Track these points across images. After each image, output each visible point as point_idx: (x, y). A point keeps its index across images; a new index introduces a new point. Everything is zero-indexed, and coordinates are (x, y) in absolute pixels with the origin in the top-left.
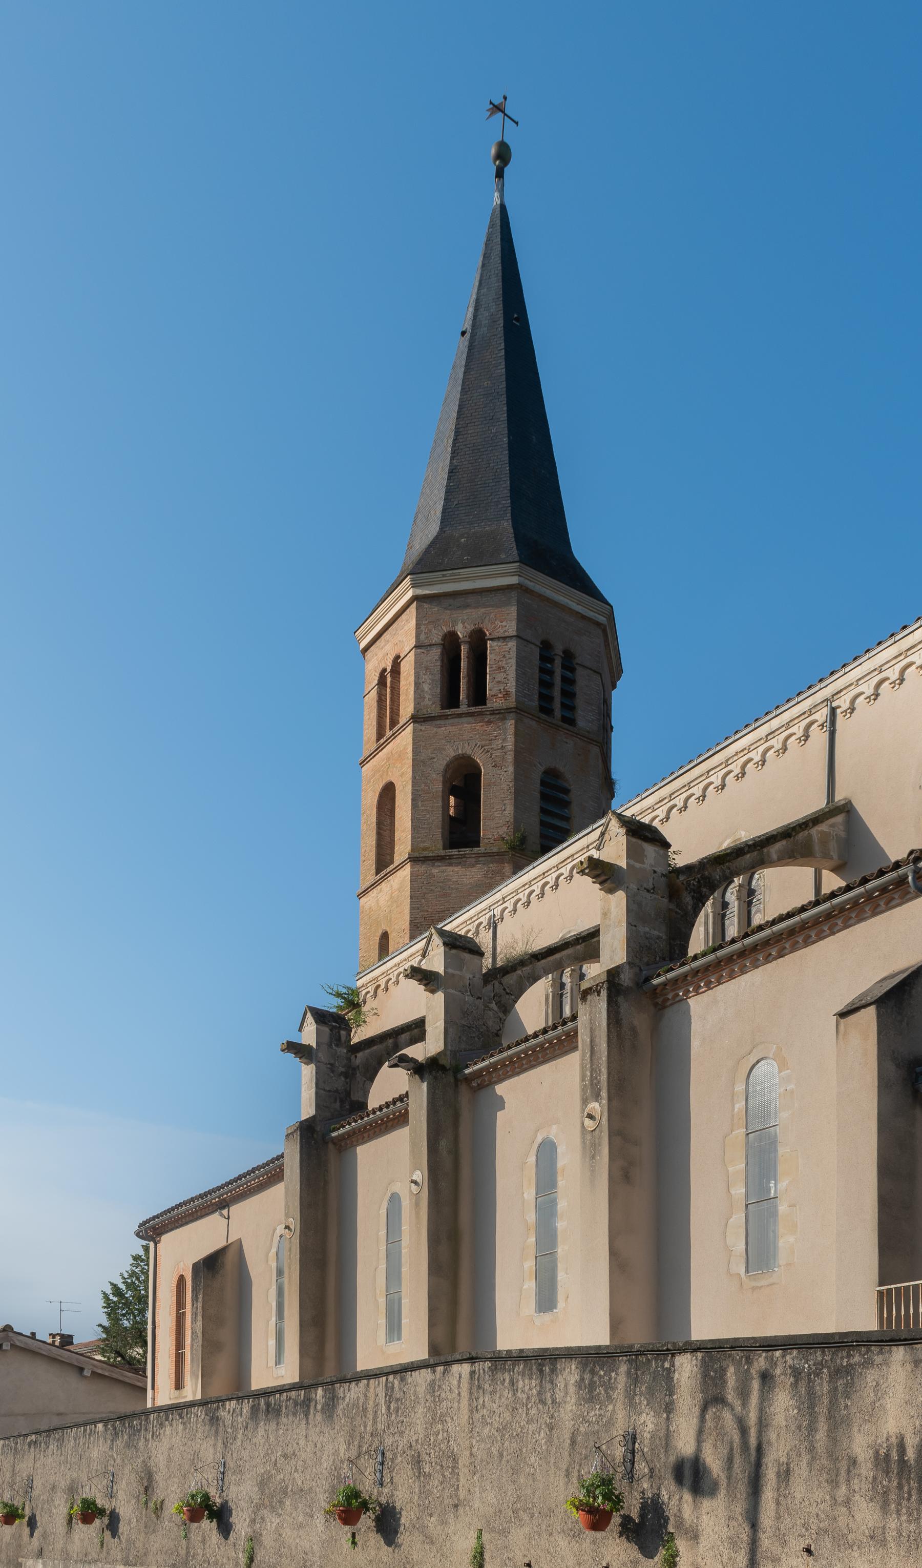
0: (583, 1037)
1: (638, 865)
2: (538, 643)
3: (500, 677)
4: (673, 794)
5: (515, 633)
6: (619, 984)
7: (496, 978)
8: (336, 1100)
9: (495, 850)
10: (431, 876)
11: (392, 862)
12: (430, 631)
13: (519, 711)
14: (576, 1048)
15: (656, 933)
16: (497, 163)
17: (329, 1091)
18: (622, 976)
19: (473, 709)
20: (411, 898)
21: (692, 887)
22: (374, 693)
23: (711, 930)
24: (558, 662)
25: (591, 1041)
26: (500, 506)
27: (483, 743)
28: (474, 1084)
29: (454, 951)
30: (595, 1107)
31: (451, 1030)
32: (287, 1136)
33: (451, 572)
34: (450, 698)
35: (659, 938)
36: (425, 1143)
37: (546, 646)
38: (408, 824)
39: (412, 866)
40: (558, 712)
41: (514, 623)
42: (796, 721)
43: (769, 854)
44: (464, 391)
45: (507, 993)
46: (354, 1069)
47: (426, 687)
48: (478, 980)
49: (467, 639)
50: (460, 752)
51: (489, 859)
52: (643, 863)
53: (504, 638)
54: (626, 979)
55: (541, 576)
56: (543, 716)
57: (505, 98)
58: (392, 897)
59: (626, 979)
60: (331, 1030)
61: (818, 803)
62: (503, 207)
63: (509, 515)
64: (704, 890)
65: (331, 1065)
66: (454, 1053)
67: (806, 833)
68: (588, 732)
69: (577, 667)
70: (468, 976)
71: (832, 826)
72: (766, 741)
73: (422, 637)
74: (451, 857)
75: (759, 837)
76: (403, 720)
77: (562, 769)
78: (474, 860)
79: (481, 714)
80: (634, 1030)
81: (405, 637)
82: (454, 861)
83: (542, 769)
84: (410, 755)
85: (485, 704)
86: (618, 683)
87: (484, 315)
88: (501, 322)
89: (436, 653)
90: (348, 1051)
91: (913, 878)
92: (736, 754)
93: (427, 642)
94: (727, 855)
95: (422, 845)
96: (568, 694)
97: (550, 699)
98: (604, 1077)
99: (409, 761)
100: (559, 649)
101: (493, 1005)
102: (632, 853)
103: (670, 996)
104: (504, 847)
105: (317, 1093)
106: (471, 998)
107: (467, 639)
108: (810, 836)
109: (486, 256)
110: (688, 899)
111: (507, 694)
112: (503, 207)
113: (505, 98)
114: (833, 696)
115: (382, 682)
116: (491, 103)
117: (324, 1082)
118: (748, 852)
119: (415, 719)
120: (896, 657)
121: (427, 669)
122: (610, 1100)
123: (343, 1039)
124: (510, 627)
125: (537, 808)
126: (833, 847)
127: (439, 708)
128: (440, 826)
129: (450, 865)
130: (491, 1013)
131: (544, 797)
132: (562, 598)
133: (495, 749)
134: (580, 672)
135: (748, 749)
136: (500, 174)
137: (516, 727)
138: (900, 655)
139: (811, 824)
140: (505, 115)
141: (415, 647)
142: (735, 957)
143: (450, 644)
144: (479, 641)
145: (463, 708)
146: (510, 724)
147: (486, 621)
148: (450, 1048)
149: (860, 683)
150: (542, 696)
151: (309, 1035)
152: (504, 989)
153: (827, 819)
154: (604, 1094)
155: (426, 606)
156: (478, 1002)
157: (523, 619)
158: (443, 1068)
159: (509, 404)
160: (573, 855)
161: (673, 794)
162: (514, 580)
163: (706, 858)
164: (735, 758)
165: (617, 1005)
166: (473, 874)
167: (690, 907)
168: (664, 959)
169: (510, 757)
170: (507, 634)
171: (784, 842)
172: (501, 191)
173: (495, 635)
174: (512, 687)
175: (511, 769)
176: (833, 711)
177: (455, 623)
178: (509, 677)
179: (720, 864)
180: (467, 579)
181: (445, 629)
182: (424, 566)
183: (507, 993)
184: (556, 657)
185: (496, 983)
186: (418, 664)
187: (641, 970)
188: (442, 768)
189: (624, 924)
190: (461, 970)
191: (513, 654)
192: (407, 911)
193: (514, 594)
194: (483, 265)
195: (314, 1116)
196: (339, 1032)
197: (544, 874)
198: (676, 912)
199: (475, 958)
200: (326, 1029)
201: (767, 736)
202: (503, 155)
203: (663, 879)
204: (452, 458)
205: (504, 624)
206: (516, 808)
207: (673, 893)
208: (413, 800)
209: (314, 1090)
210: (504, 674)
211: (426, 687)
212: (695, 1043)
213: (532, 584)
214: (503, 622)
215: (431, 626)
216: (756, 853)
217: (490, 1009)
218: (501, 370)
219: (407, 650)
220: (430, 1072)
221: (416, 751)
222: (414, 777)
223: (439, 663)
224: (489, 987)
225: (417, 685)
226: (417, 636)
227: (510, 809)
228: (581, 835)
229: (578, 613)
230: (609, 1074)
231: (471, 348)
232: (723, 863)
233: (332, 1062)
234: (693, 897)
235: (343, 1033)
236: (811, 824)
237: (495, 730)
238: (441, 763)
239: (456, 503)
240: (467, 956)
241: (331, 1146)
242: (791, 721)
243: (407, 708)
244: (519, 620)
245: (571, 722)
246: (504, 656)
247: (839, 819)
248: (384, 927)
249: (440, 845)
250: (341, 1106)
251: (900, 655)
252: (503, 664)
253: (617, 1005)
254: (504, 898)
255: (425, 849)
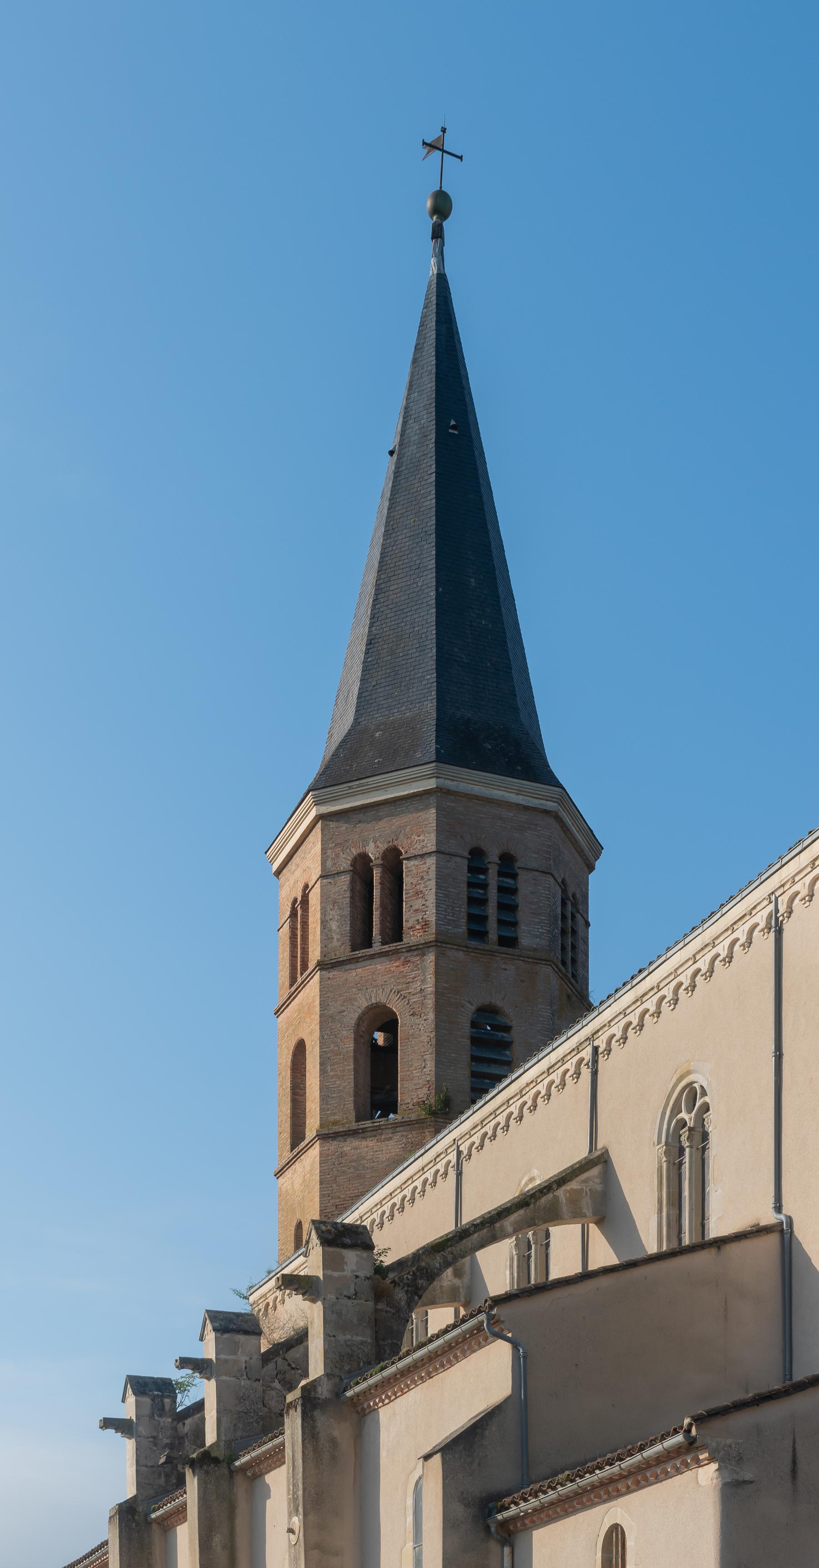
0: (288, 1452)
1: (336, 1274)
2: (466, 854)
3: (418, 904)
4: (484, 1120)
5: (434, 849)
6: (315, 1398)
7: (278, 1355)
8: (160, 1475)
9: (413, 1117)
10: (343, 1155)
11: (303, 1139)
12: (337, 856)
13: (441, 943)
14: (284, 1463)
15: (359, 1338)
16: (435, 218)
17: (152, 1467)
18: (319, 1390)
19: (386, 948)
20: (321, 1183)
21: (405, 1281)
22: (286, 927)
23: (515, 1275)
24: (493, 871)
25: (293, 1456)
26: (424, 682)
27: (400, 987)
28: (249, 1474)
29: (226, 1336)
30: (295, 1519)
31: (224, 1419)
32: (110, 1518)
33: (358, 783)
34: (361, 938)
35: (362, 1343)
36: (197, 1542)
37: (477, 854)
38: (317, 1094)
39: (321, 1146)
40: (493, 936)
41: (433, 837)
42: (569, 1057)
43: (502, 1229)
44: (387, 534)
45: (293, 1369)
46: (183, 1438)
47: (334, 925)
48: (256, 1361)
49: (380, 862)
50: (374, 1001)
51: (407, 1128)
52: (343, 1270)
53: (422, 856)
54: (324, 1392)
55: (465, 772)
56: (474, 943)
57: (444, 130)
58: (304, 1181)
59: (324, 1392)
60: (153, 1400)
61: (581, 1152)
62: (442, 280)
63: (434, 693)
64: (420, 1282)
65: (154, 1437)
66: (228, 1443)
67: (550, 1196)
68: (535, 950)
69: (519, 871)
70: (243, 1358)
71: (585, 1181)
72: (549, 1075)
73: (329, 863)
74: (364, 1130)
75: (489, 1212)
76: (312, 965)
77: (499, 1003)
78: (391, 1131)
79: (396, 952)
80: (333, 1442)
81: (309, 865)
82: (369, 1134)
83: (473, 1008)
84: (317, 1009)
85: (402, 940)
86: (598, 864)
87: (414, 427)
88: (433, 436)
89: (345, 880)
90: (173, 1420)
91: (487, 1325)
92: (528, 1085)
93: (334, 870)
94: (448, 1240)
95: (332, 1118)
96: (508, 908)
97: (483, 919)
98: (300, 1493)
99: (317, 1017)
100: (493, 856)
101: (277, 1384)
102: (328, 1263)
103: (365, 1406)
104: (423, 1114)
105: (137, 1471)
106: (248, 1382)
107: (380, 862)
108: (556, 1198)
109: (418, 348)
110: (400, 1295)
111: (426, 924)
112: (442, 280)
113: (444, 130)
114: (593, 1035)
115: (293, 914)
116: (424, 143)
117: (146, 1458)
118: (475, 1232)
119: (322, 966)
120: (634, 1003)
121: (334, 902)
122: (305, 1515)
123: (167, 1407)
124: (429, 841)
125: (466, 1058)
126: (586, 1205)
127: (349, 948)
128: (352, 1093)
129: (365, 1138)
130: (273, 1393)
131: (475, 1041)
132: (495, 792)
133: (410, 987)
134: (523, 876)
135: (535, 1082)
136: (438, 233)
137: (436, 964)
138: (637, 1000)
139: (555, 1186)
140: (443, 151)
141: (321, 877)
142: (398, 1376)
143: (361, 868)
144: (394, 863)
145: (377, 947)
146: (430, 958)
147: (402, 836)
148: (223, 1438)
149: (612, 1024)
150: (471, 918)
151: (128, 1410)
152: (289, 1365)
153: (577, 1176)
154: (301, 1510)
155: (332, 825)
156: (255, 1384)
157: (444, 829)
158: (216, 1461)
159: (438, 546)
160: (412, 1177)
161: (484, 1120)
162: (431, 784)
163: (421, 1248)
164: (527, 1089)
165: (313, 1420)
166: (391, 1146)
167: (403, 1303)
168: (369, 1363)
169: (430, 1002)
170: (425, 850)
171: (521, 1212)
172: (440, 256)
173: (412, 852)
174: (433, 919)
175: (431, 1016)
176: (596, 1049)
177: (366, 842)
178: (428, 903)
179: (439, 1252)
180: (377, 789)
181: (355, 852)
182: (333, 776)
183: (293, 1369)
184: (489, 866)
185: (279, 1360)
186: (324, 897)
187: (341, 1379)
188: (353, 1022)
189: (322, 1336)
190: (236, 1354)
191: (433, 875)
192: (317, 1199)
193: (433, 800)
194: (414, 361)
195: (134, 1498)
196: (162, 1401)
197: (391, 1194)
198: (386, 1312)
199: (252, 1339)
200: (147, 1400)
201: (548, 1070)
202: (442, 206)
203: (367, 1282)
204: (371, 626)
205: (421, 838)
206: (438, 1063)
207: (379, 1295)
208: (321, 1064)
209: (135, 1467)
210: (423, 902)
211: (334, 925)
212: (383, 1453)
213: (455, 783)
214: (420, 834)
215: (338, 850)
216: (485, 1231)
217: (273, 1389)
218: (430, 501)
219: (314, 878)
220: (201, 1467)
221: (323, 1006)
222: (322, 1037)
223: (348, 894)
224: (271, 1365)
225: (324, 923)
226: (323, 863)
227: (430, 1065)
228: (394, 1174)
229: (518, 805)
230: (304, 1490)
231: (397, 473)
232: (443, 1250)
233: (155, 1434)
234: (407, 1292)
235: (167, 1401)
236: (555, 1186)
237: (413, 970)
238: (352, 1017)
239: (373, 683)
240: (242, 1338)
241: (155, 1526)
242: (564, 1057)
243: (315, 954)
244: (439, 831)
245: (508, 942)
246: (422, 878)
247: (595, 1171)
248: (298, 1216)
249: (352, 1116)
250: (166, 1482)
251: (637, 1000)
252: (421, 887)
253: (313, 1420)
254: (361, 1217)
255: (335, 1123)
